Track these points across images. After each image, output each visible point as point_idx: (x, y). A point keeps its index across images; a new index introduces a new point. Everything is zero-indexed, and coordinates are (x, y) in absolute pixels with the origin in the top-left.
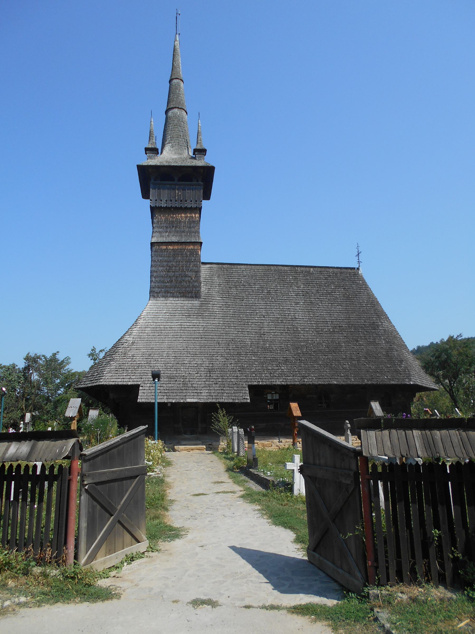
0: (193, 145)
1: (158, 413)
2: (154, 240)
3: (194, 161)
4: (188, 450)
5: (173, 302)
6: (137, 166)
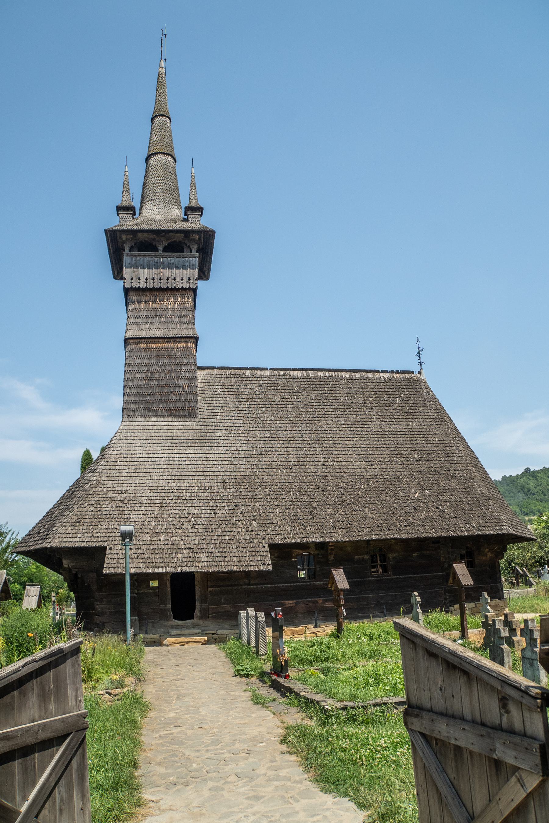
0: (185, 203)
1: (131, 589)
2: (130, 334)
3: (186, 223)
4: (181, 644)
5: (156, 423)
6: (106, 231)
